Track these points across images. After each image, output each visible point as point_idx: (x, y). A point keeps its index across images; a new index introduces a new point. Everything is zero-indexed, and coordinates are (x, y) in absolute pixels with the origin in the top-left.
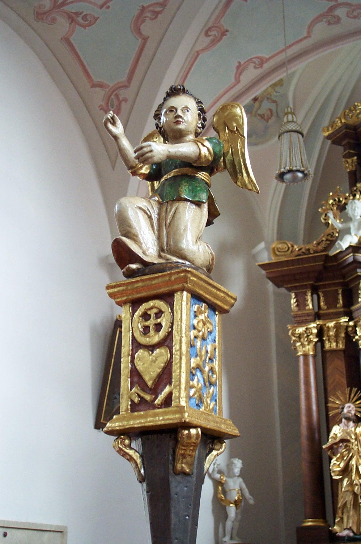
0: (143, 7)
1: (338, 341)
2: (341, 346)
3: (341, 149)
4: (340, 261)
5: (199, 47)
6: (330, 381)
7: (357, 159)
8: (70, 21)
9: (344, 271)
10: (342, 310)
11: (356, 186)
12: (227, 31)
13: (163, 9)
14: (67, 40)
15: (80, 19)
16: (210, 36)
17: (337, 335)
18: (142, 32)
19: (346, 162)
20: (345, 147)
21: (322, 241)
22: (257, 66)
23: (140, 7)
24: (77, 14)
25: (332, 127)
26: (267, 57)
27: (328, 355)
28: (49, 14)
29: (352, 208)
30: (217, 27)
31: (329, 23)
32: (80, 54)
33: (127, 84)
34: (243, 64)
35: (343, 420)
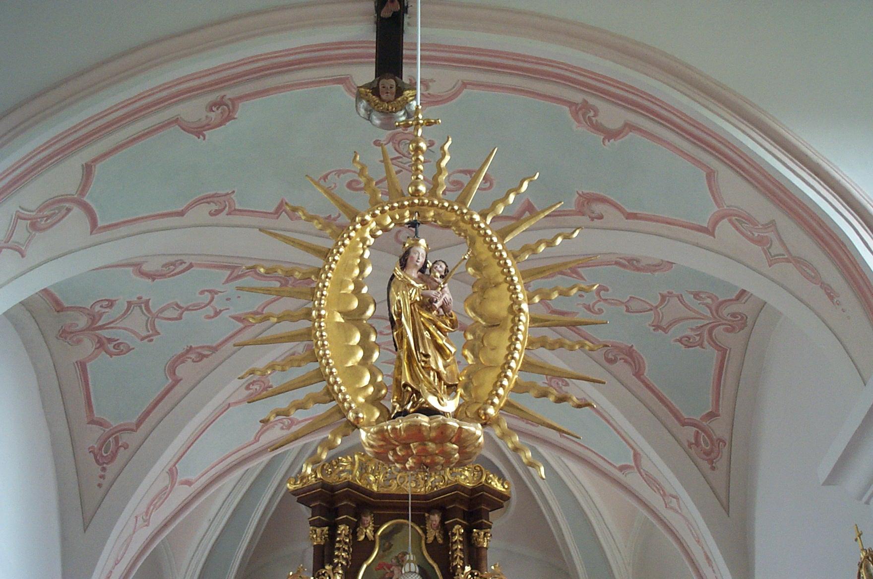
0: (191, 347)
5: (232, 400)
7: (329, 530)
11: (324, 568)
13: (212, 354)
14: (82, 366)
15: (110, 347)
18: (176, 373)
19: (314, 532)
22: (284, 427)
23: (187, 347)
24: (110, 340)
30: (263, 382)
33: (135, 428)
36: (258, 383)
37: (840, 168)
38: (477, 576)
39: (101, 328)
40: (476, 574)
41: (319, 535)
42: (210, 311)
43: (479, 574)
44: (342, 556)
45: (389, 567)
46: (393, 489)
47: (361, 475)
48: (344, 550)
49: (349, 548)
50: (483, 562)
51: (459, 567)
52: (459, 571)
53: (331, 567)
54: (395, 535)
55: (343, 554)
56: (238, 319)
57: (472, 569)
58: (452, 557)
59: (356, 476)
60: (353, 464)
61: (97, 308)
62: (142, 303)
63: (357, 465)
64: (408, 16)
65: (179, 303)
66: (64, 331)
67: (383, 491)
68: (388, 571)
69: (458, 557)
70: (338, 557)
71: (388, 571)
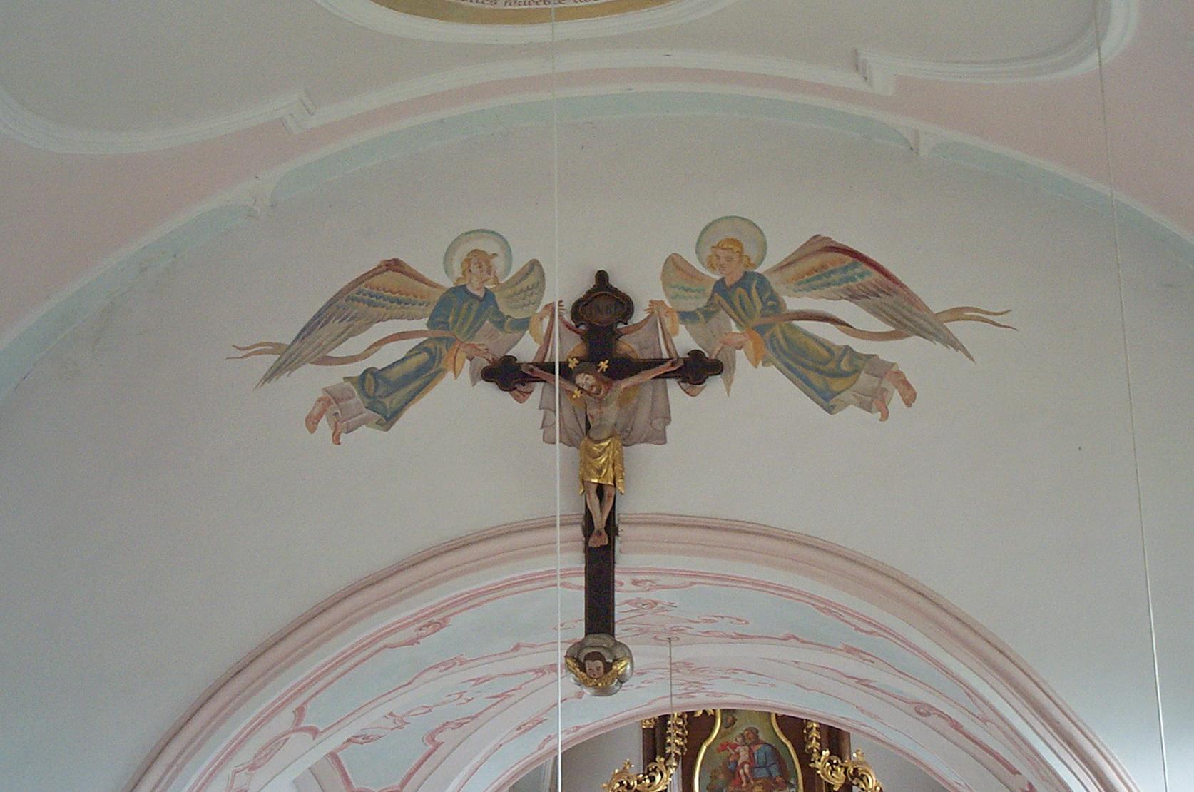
37: (1097, 734)
38: (837, 764)
40: (835, 762)
43: (839, 761)
45: (734, 747)
50: (846, 741)
51: (815, 750)
52: (815, 756)
53: (663, 760)
55: (676, 741)
57: (830, 755)
58: (807, 738)
64: (620, 538)
68: (733, 753)
69: (814, 739)
70: (669, 745)
71: (733, 753)
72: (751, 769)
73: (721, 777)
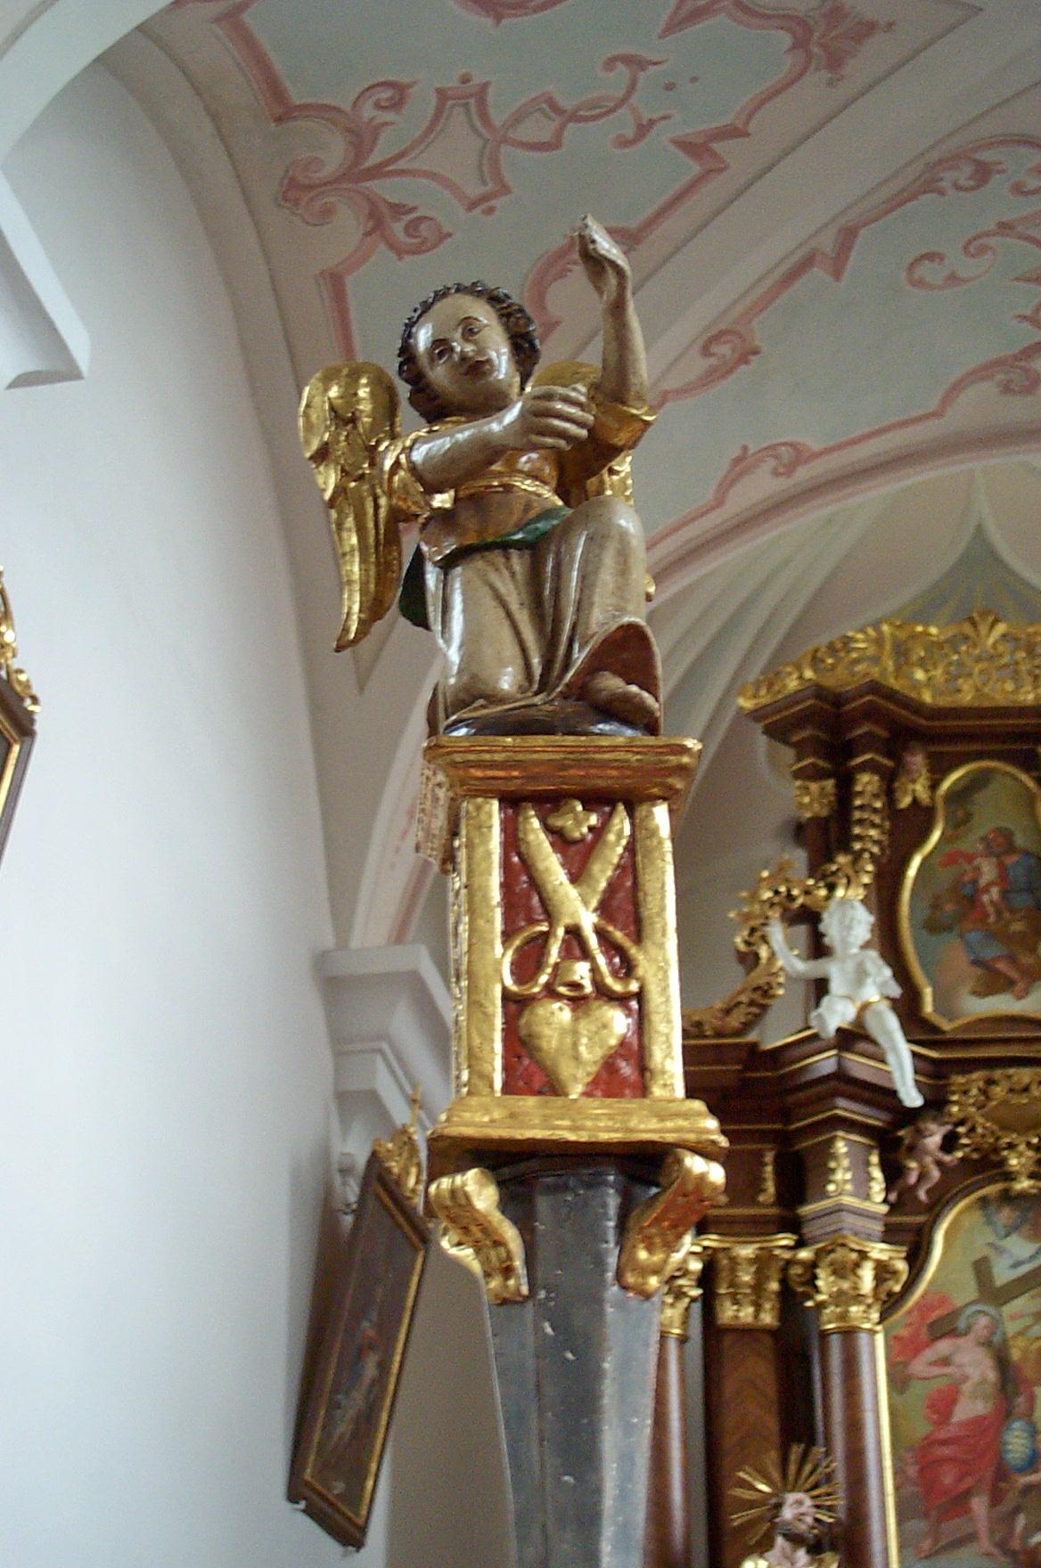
1: (761, 1301)
2: (768, 1318)
3: (788, 754)
4: (782, 1072)
6: (729, 1420)
8: (371, 224)
9: (791, 1099)
10: (774, 1211)
12: (756, 352)
14: (335, 283)
15: (398, 228)
16: (712, 355)
17: (758, 1287)
18: (549, 304)
20: (801, 749)
21: (740, 1003)
24: (398, 210)
25: (770, 685)
26: (816, 446)
27: (728, 1341)
28: (323, 192)
29: (841, 922)
31: (1006, 389)
32: (355, 327)
34: (755, 453)
35: (780, 1541)
36: (729, 338)
39: (377, 172)
41: (812, 800)
42: (623, 123)
44: (871, 836)
45: (970, 858)
46: (967, 697)
47: (898, 669)
48: (874, 825)
49: (883, 819)
54: (976, 796)
56: (690, 147)
59: (885, 669)
60: (879, 641)
61: (368, 111)
62: (471, 95)
63: (888, 646)
65: (557, 96)
66: (293, 184)
67: (945, 701)
68: (968, 867)
70: (859, 838)
72: (1005, 894)
73: (949, 907)
